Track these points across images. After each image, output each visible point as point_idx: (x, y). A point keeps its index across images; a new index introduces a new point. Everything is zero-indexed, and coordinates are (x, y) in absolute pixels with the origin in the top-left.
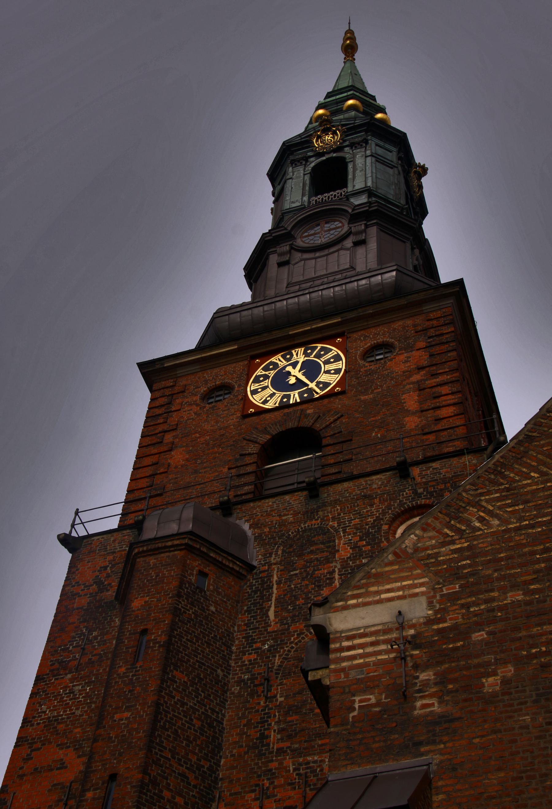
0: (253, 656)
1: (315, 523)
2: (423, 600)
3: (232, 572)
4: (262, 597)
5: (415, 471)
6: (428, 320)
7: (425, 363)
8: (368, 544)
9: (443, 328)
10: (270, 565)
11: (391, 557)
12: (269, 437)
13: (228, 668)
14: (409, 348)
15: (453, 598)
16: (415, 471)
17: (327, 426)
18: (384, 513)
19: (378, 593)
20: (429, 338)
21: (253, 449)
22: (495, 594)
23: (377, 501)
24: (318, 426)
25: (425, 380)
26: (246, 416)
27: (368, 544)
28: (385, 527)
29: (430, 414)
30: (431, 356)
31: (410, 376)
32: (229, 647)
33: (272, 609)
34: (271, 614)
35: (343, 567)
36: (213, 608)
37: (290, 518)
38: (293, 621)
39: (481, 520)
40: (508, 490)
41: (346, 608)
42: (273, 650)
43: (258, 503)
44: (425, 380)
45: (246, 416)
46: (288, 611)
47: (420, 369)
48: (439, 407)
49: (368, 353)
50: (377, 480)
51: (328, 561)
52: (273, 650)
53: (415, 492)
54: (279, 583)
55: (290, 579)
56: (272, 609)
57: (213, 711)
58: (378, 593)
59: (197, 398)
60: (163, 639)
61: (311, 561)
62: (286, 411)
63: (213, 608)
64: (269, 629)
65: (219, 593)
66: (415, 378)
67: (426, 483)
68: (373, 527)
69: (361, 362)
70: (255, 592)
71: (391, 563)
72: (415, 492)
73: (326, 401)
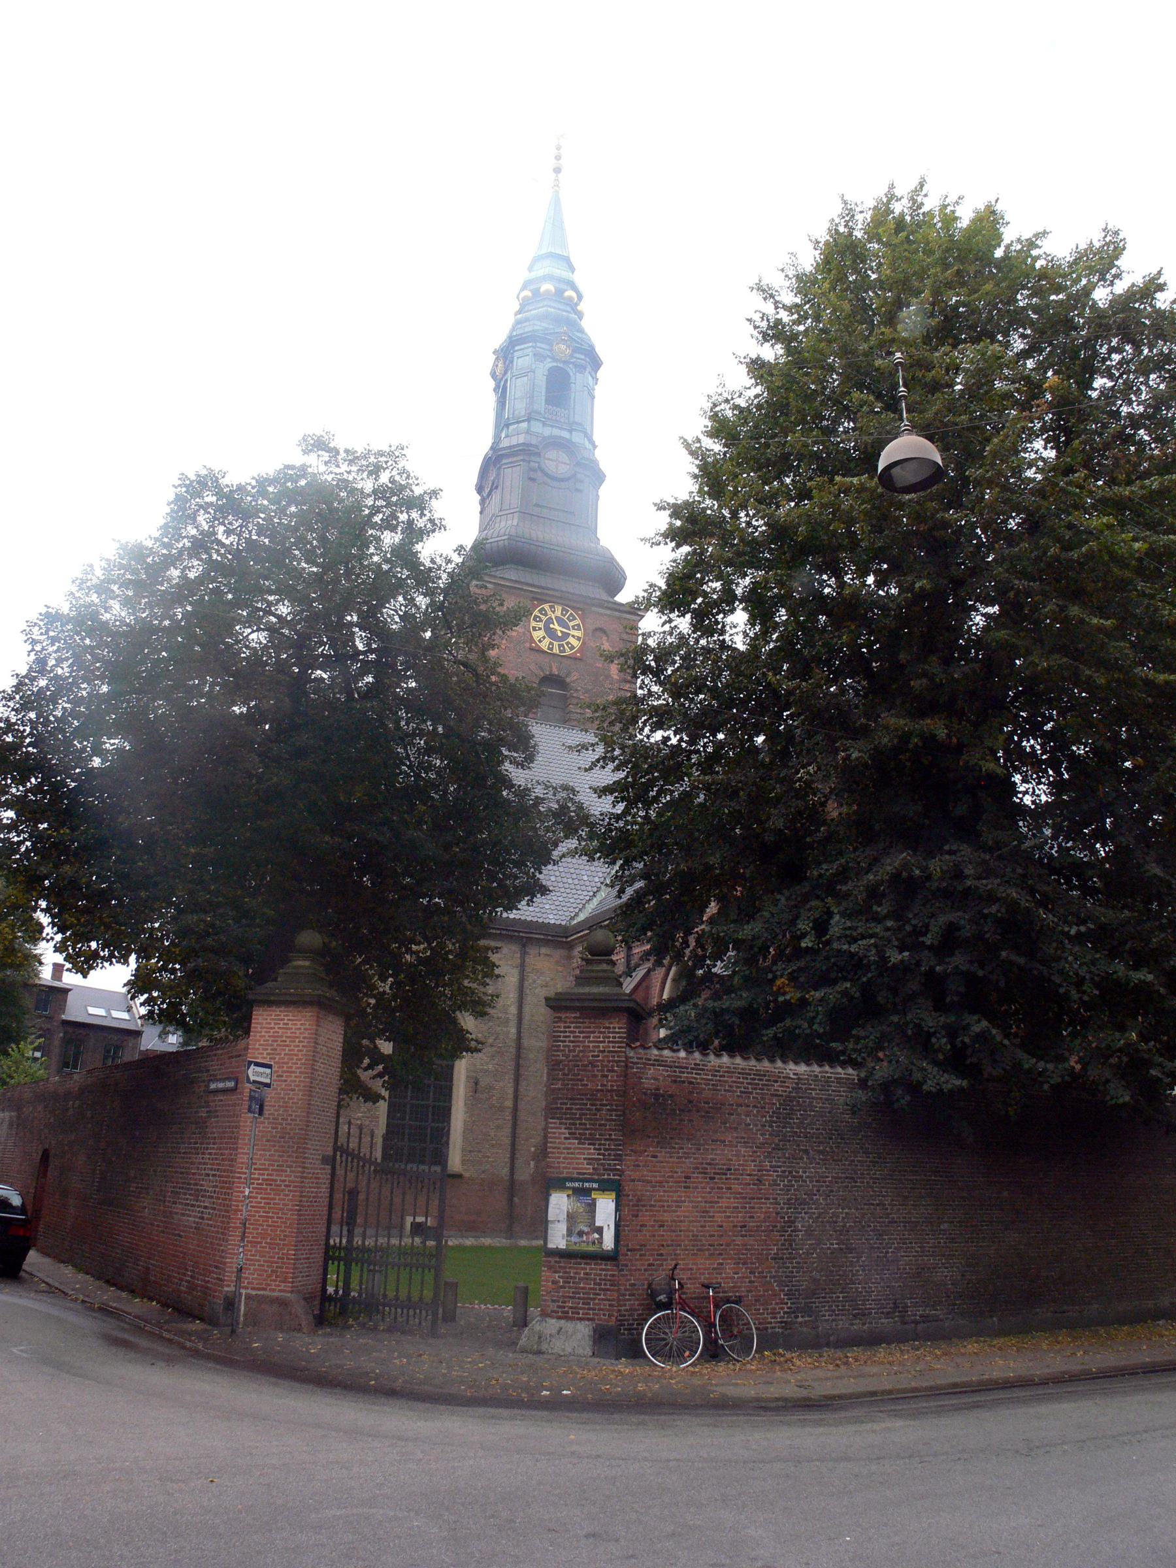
24: (568, 680)
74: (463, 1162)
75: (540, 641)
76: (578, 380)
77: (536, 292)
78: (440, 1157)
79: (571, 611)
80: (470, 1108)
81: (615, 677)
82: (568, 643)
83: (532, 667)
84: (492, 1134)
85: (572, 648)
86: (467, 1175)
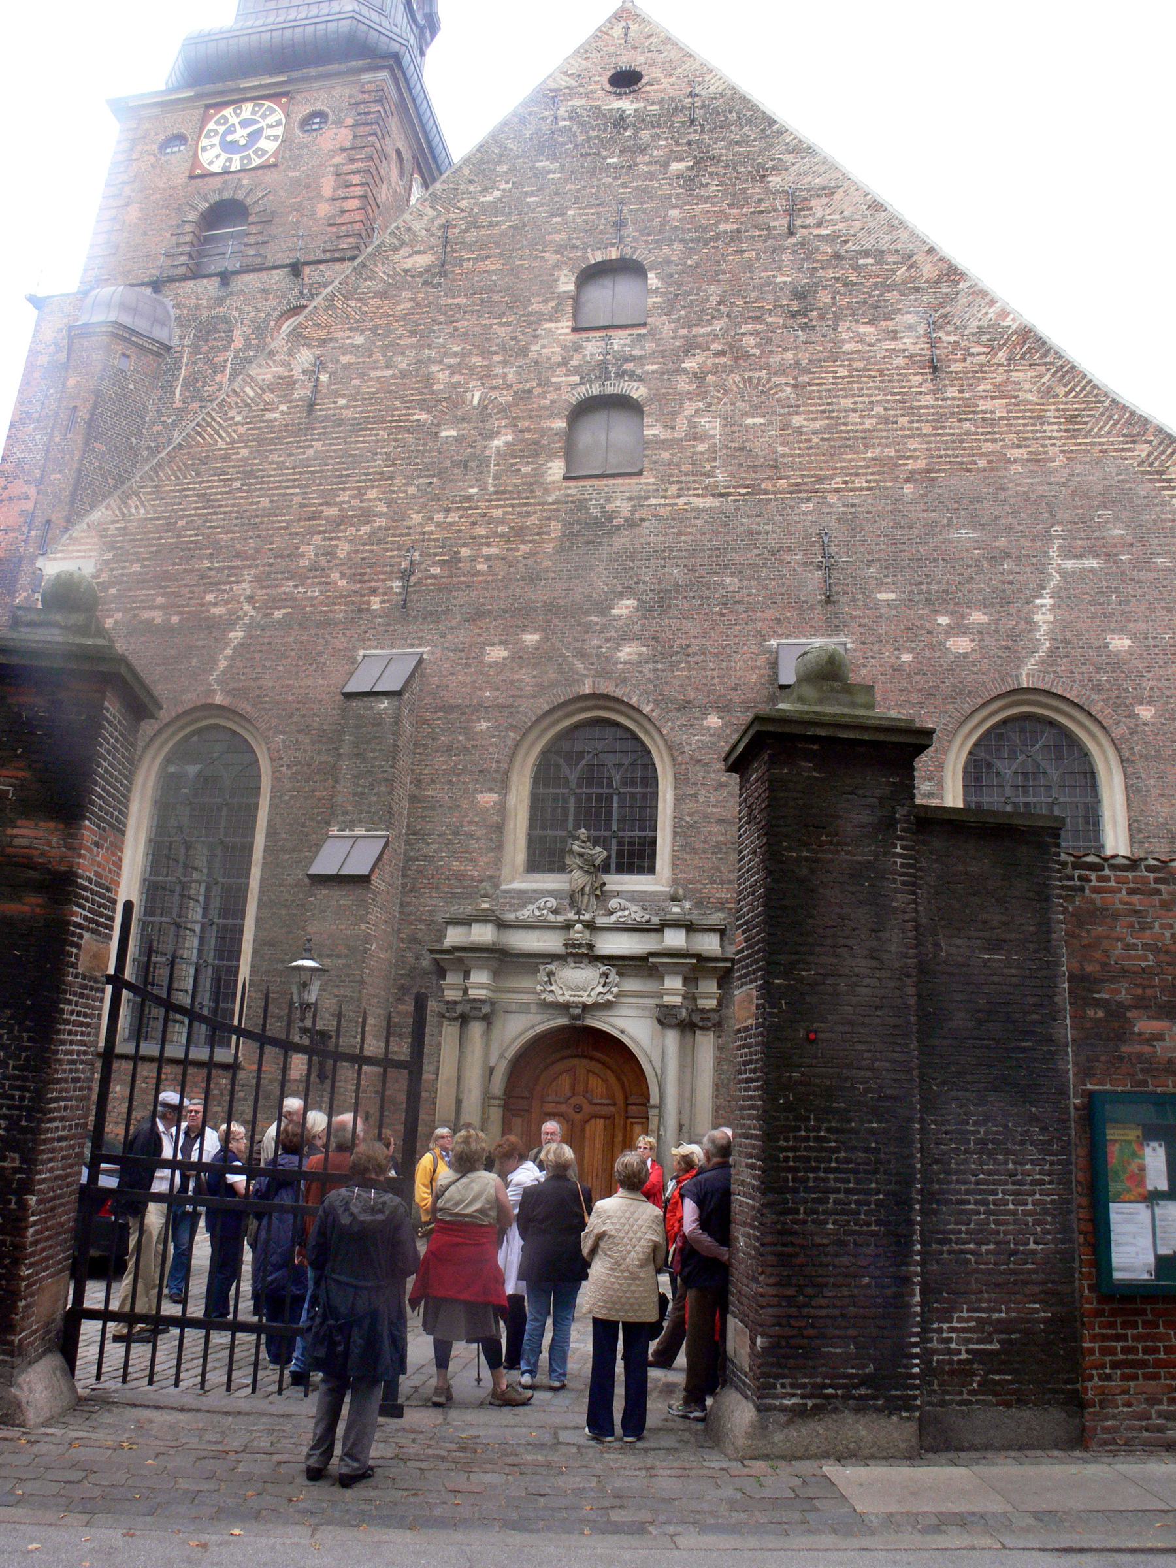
0: (160, 428)
1: (221, 311)
2: (93, 560)
3: (152, 352)
4: (173, 375)
5: (307, 270)
6: (363, 92)
7: (348, 145)
8: (257, 338)
9: (373, 105)
10: (183, 346)
11: (85, 526)
12: (207, 205)
13: (140, 436)
14: (339, 123)
15: (107, 562)
16: (307, 270)
17: (256, 202)
18: (274, 309)
19: (72, 551)
20: (359, 114)
21: (193, 216)
22: (127, 564)
23: (271, 296)
24: (248, 201)
25: (343, 165)
26: (192, 177)
27: (257, 338)
28: (272, 324)
29: (338, 204)
30: (355, 136)
31: (333, 157)
32: (143, 418)
33: (179, 388)
34: (178, 392)
35: (235, 357)
36: (131, 387)
37: (204, 302)
38: (192, 402)
39: (137, 507)
40: (156, 486)
41: (55, 559)
42: (174, 424)
43: (183, 284)
44: (343, 165)
45: (192, 177)
46: (189, 391)
47: (343, 150)
48: (346, 198)
49: (305, 122)
50: (277, 275)
51: (225, 349)
52: (174, 424)
53: (301, 292)
54: (187, 365)
55: (195, 363)
56: (179, 388)
57: (126, 471)
58: (72, 551)
59: (155, 147)
60: (87, 417)
61: (212, 348)
62: (226, 177)
63: (131, 387)
64: (175, 406)
65: (138, 372)
66: (338, 160)
67: (311, 285)
68: (263, 322)
69: (297, 132)
70: (169, 370)
71: (83, 531)
72: (301, 292)
73: (260, 172)
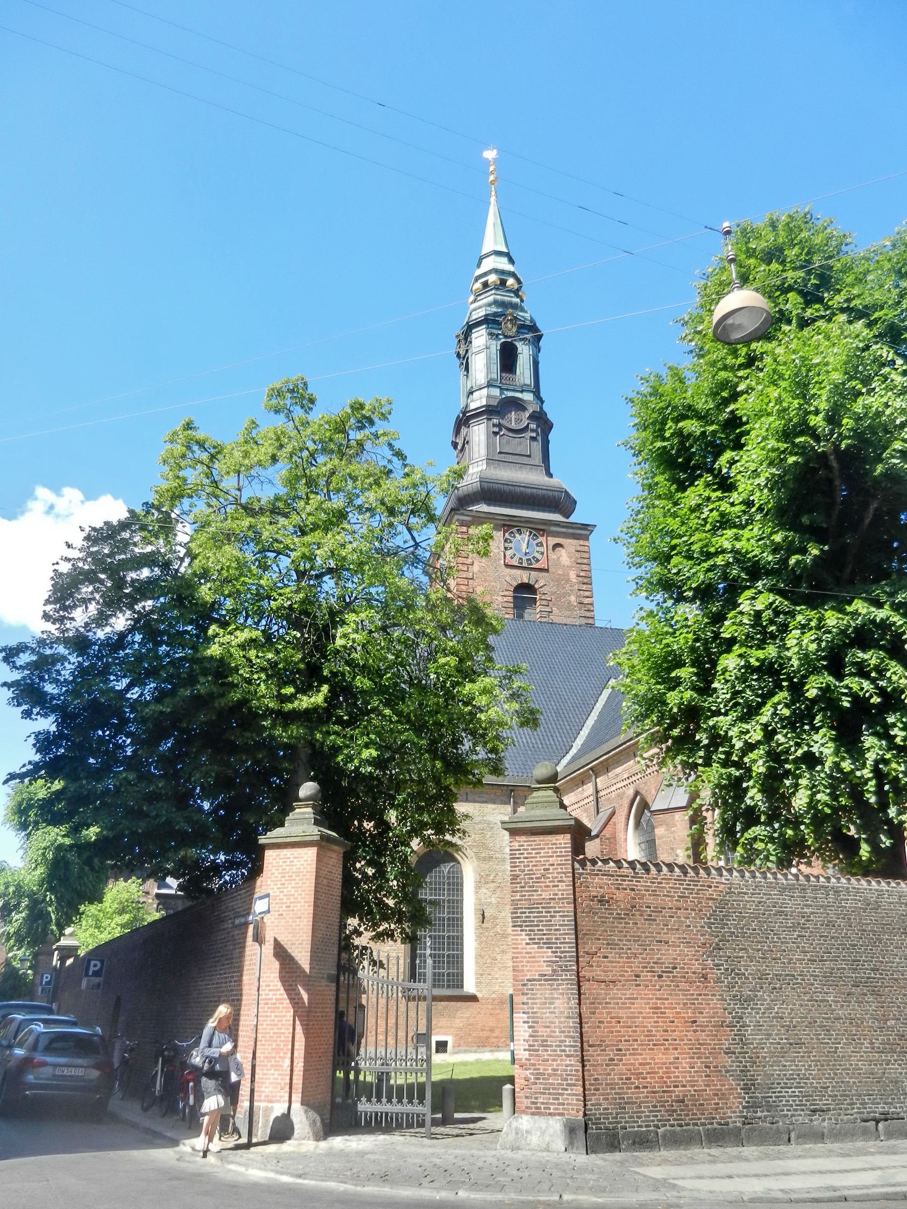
24: (536, 586)
74: (478, 984)
75: (512, 558)
76: (524, 352)
77: (485, 285)
78: (457, 980)
79: (534, 532)
80: (479, 937)
81: (574, 580)
82: (534, 557)
83: (508, 579)
84: (499, 957)
85: (538, 561)
86: (479, 995)
